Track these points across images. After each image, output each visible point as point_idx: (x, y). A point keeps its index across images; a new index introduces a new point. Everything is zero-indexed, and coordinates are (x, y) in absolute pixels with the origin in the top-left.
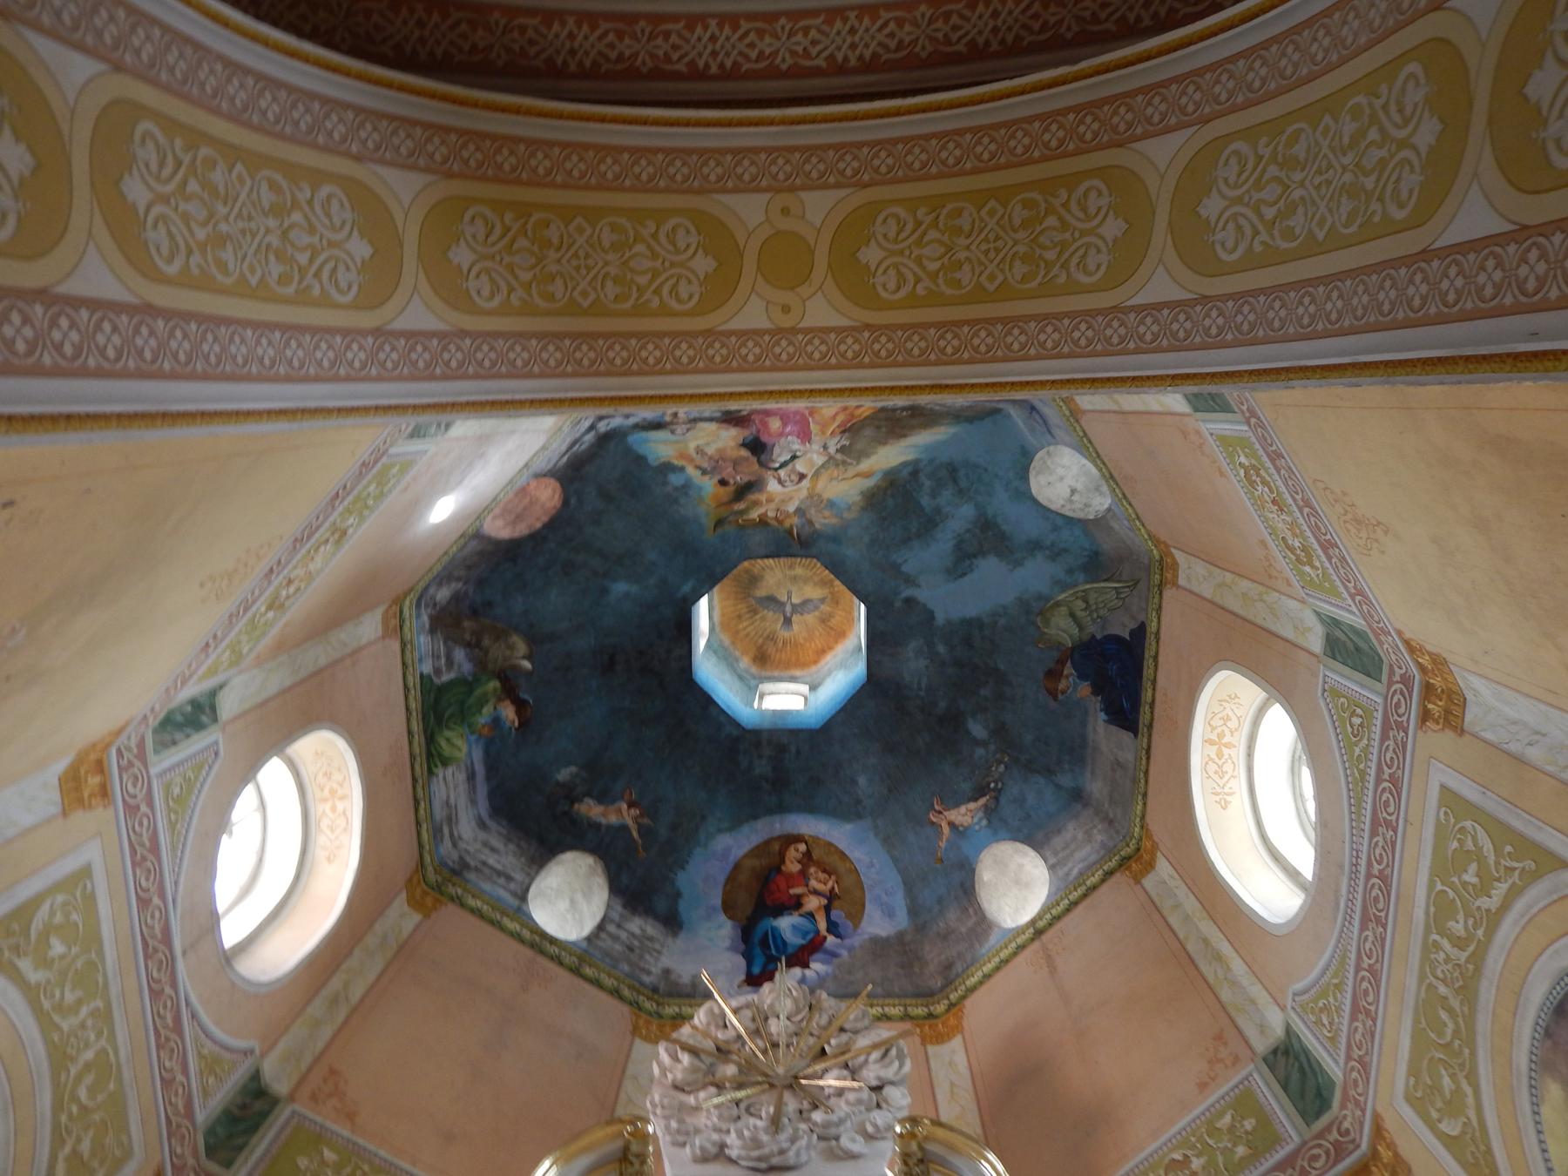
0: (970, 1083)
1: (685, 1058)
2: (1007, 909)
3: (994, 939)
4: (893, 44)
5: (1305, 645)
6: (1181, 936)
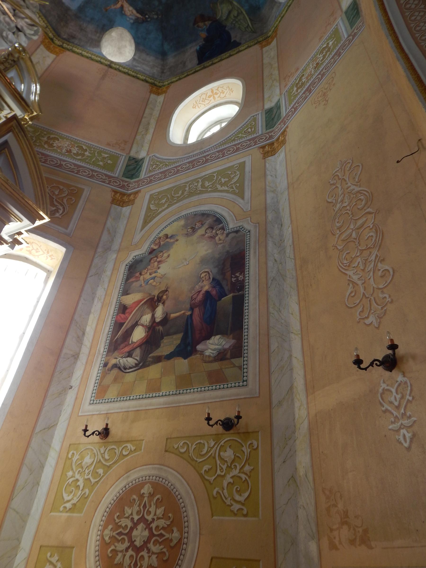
0: (45, 68)
2: (108, 50)
3: (95, 50)
5: (265, 103)
6: (145, 115)
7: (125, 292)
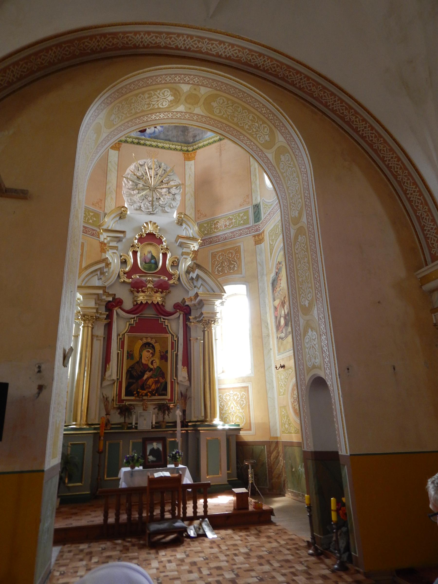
1: (131, 183)
4: (236, 55)
6: (251, 164)
7: (274, 300)
